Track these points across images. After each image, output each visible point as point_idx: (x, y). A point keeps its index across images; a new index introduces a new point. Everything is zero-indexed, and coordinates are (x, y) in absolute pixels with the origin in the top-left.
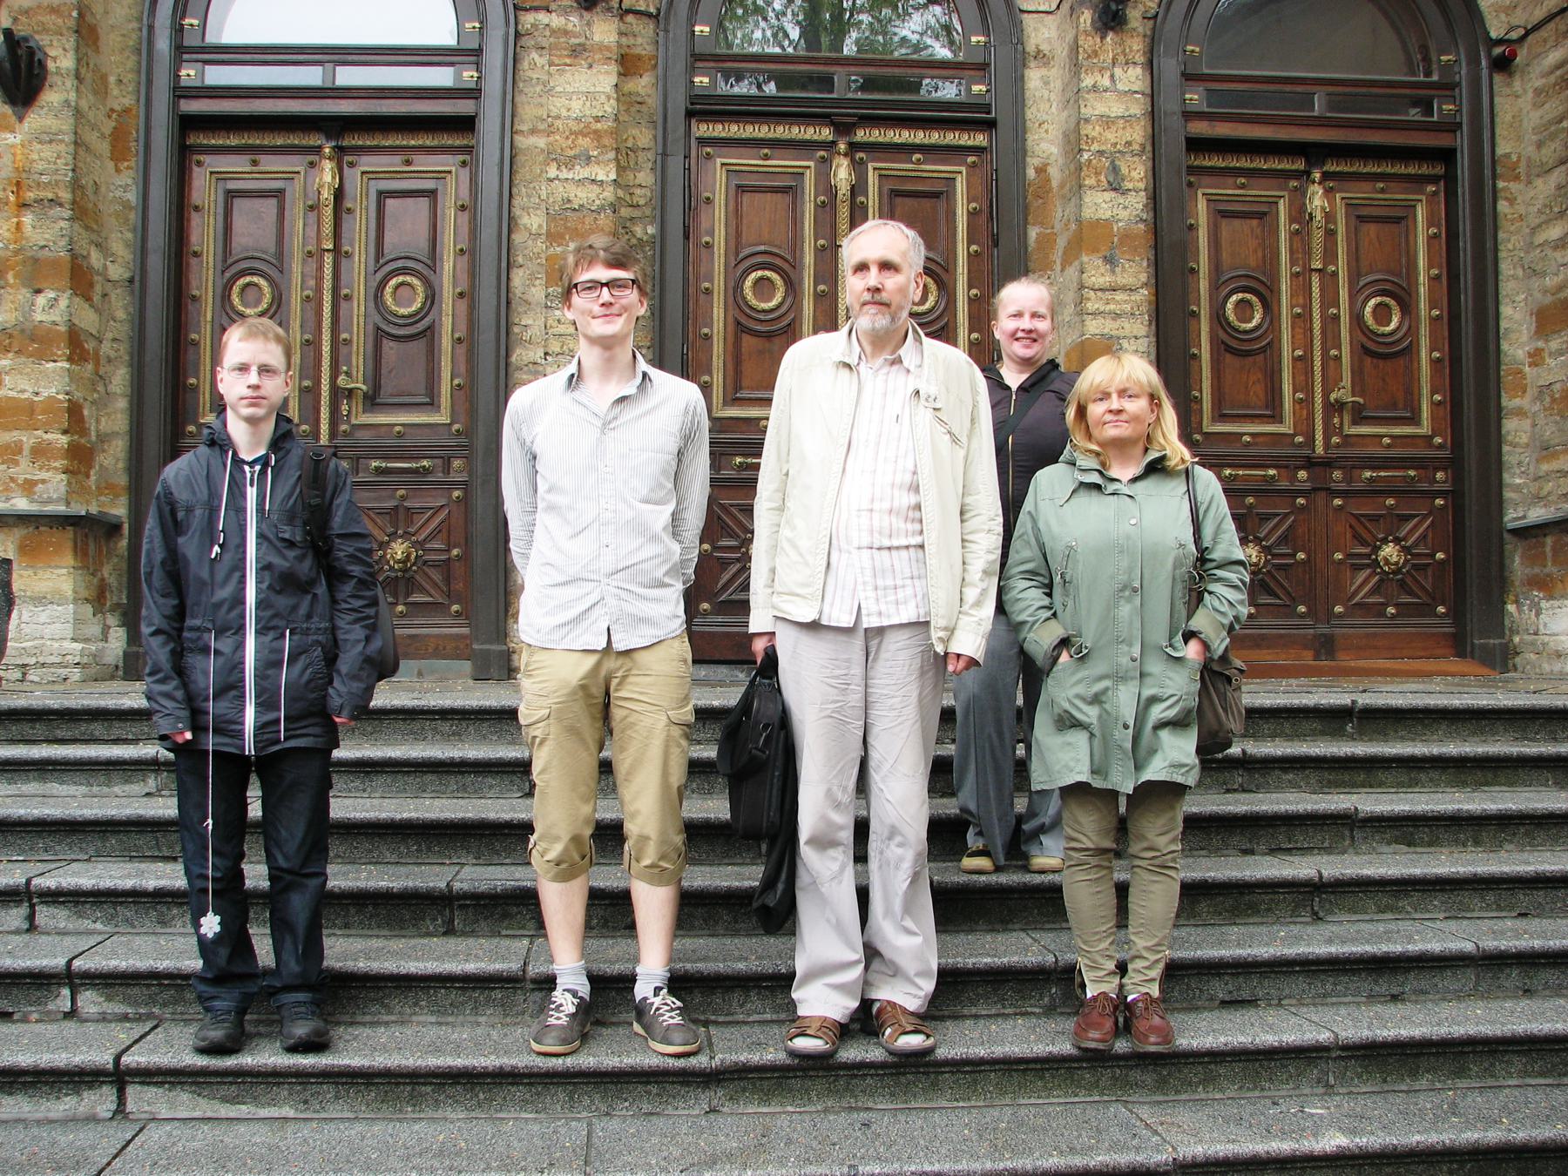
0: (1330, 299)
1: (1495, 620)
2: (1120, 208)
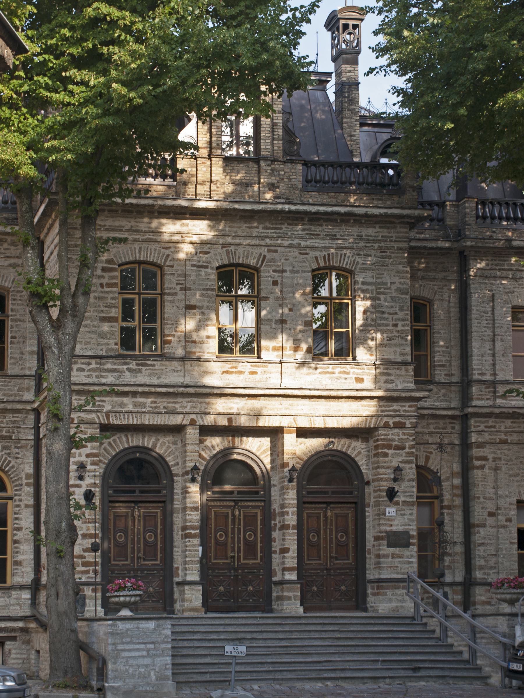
0: (331, 534)
1: (365, 602)
2: (291, 519)
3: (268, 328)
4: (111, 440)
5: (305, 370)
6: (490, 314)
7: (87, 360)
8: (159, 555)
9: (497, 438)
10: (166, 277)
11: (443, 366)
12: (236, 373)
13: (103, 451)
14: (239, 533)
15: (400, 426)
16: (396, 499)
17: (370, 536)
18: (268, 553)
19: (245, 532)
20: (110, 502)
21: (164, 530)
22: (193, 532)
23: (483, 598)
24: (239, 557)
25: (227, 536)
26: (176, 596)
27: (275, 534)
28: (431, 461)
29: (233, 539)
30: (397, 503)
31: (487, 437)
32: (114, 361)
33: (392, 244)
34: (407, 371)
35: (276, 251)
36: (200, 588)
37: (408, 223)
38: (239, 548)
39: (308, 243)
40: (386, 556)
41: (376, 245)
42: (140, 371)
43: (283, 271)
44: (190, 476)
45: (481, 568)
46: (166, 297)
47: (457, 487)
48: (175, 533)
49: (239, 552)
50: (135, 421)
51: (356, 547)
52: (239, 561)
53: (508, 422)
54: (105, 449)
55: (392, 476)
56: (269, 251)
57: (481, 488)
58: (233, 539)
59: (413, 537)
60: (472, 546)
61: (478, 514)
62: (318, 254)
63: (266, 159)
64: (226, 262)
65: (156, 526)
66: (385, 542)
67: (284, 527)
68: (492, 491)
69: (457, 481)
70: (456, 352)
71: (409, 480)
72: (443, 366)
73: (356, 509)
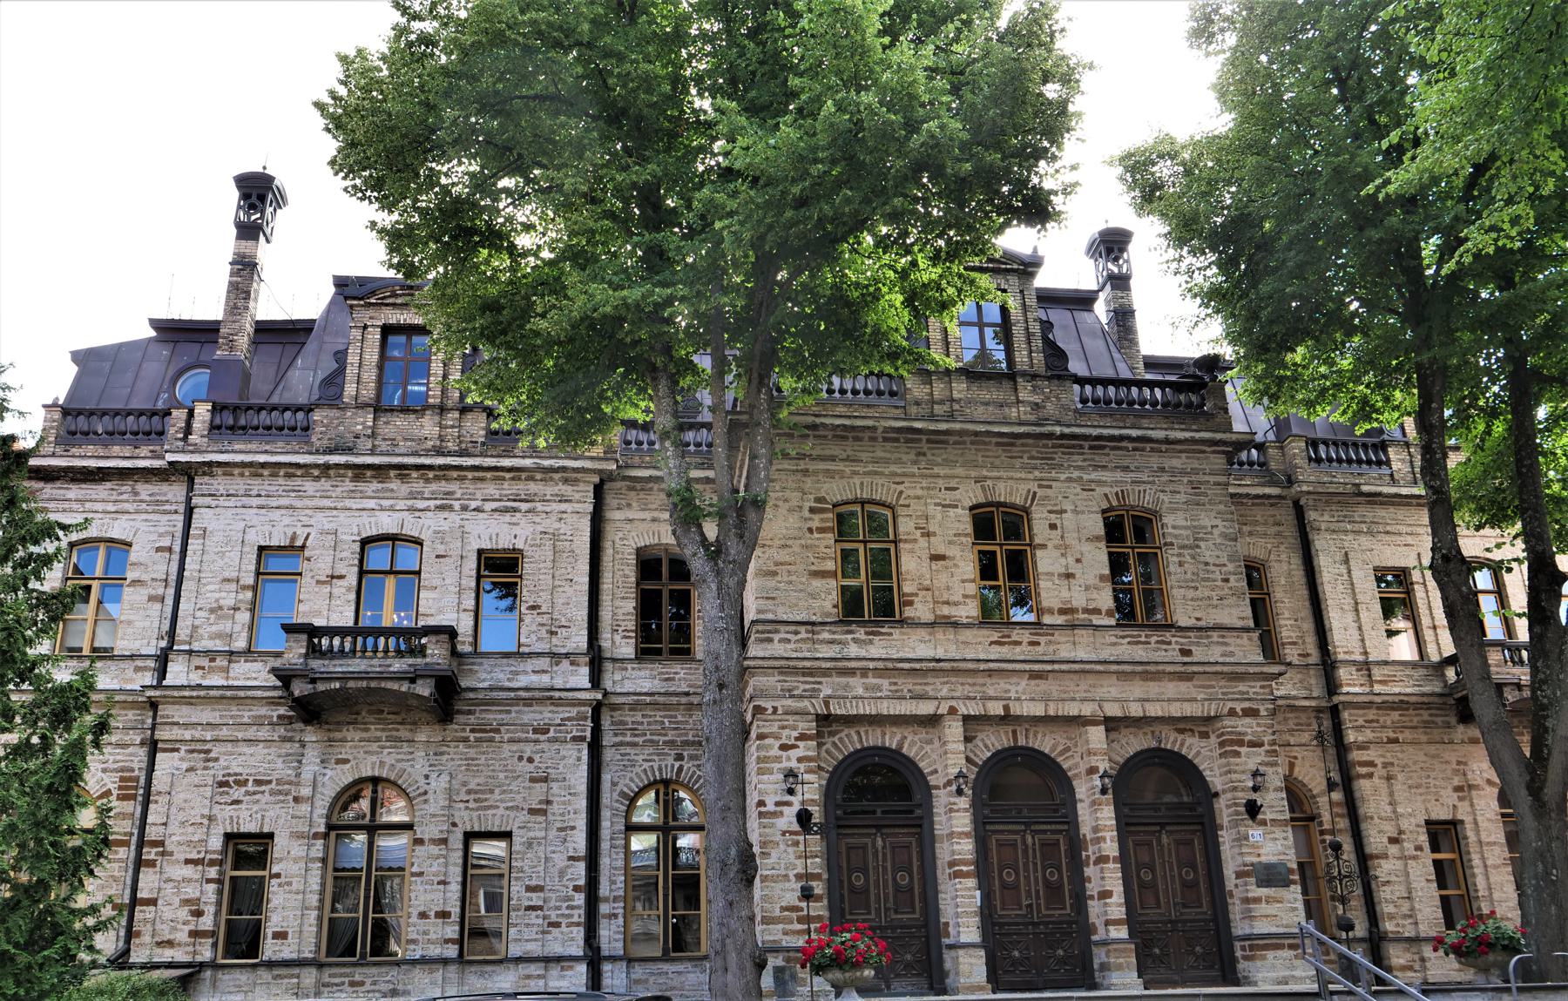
0: (1171, 870)
1: (1234, 970)
2: (1111, 848)
3: (1049, 584)
4: (836, 739)
5: (1087, 60)
6: (1346, 577)
7: (793, 628)
8: (918, 906)
9: (1384, 736)
10: (901, 520)
11: (1294, 643)
12: (1009, 643)
13: (824, 754)
14: (1036, 870)
15: (1251, 713)
16: (1260, 817)
17: (1229, 871)
18: (1080, 900)
19: (1044, 869)
20: (839, 827)
21: (922, 867)
22: (965, 868)
23: (1402, 961)
24: (1039, 905)
25: (1017, 874)
26: (948, 965)
27: (1089, 871)
28: (1297, 770)
29: (1027, 878)
30: (1264, 823)
31: (1368, 735)
32: (833, 628)
33: (1207, 478)
34: (1250, 639)
35: (1050, 487)
36: (982, 953)
37: (1223, 452)
38: (1037, 892)
39: (1093, 476)
40: (1257, 900)
41: (1185, 480)
42: (871, 642)
43: (1062, 512)
44: (954, 788)
45: (1391, 917)
46: (902, 545)
47: (1338, 804)
48: (939, 872)
49: (1038, 897)
50: (867, 709)
51: (1211, 889)
52: (1039, 911)
53: (1395, 715)
54: (827, 752)
55: (1251, 784)
56: (1040, 486)
57: (1373, 805)
58: (1027, 878)
59: (1291, 871)
60: (1373, 886)
61: (1375, 839)
62: (1107, 490)
63: (1024, 374)
64: (982, 500)
65: (911, 863)
66: (1253, 880)
67: (1102, 859)
68: (1389, 809)
69: (1337, 796)
70: (1308, 626)
71: (1276, 790)
72: (1294, 643)
73: (1203, 832)
